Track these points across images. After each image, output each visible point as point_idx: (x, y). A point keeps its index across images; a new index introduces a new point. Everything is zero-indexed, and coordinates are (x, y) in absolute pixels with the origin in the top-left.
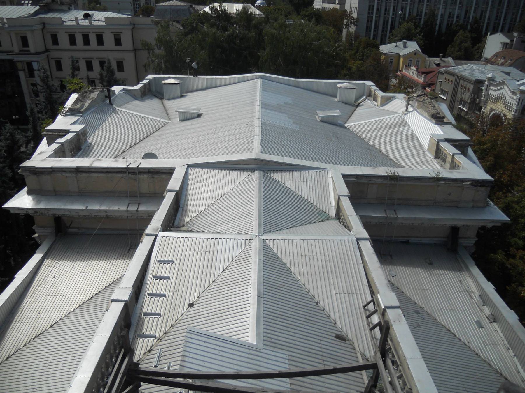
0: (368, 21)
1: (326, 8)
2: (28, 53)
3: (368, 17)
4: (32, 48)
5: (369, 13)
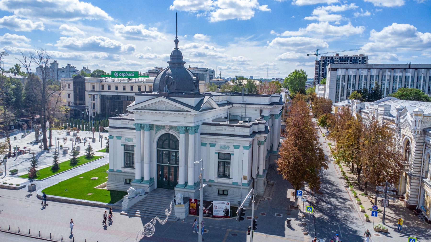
0: (336, 92)
1: (354, 57)
2: (94, 91)
3: (336, 90)
4: (95, 90)
5: (337, 88)
